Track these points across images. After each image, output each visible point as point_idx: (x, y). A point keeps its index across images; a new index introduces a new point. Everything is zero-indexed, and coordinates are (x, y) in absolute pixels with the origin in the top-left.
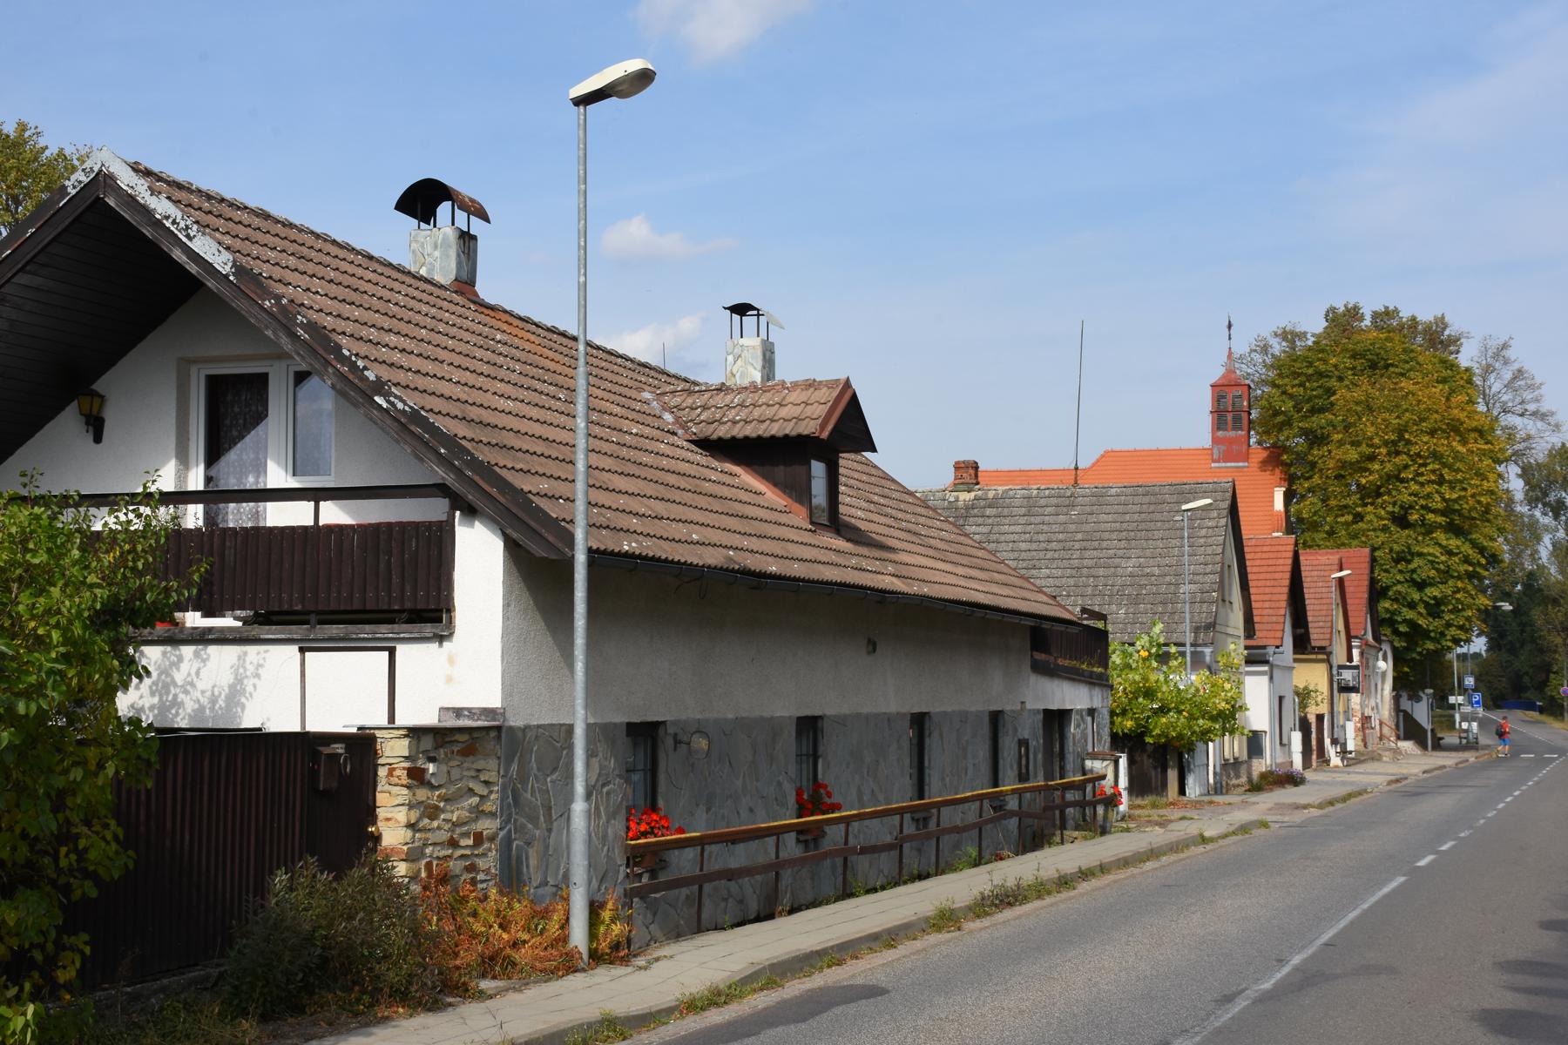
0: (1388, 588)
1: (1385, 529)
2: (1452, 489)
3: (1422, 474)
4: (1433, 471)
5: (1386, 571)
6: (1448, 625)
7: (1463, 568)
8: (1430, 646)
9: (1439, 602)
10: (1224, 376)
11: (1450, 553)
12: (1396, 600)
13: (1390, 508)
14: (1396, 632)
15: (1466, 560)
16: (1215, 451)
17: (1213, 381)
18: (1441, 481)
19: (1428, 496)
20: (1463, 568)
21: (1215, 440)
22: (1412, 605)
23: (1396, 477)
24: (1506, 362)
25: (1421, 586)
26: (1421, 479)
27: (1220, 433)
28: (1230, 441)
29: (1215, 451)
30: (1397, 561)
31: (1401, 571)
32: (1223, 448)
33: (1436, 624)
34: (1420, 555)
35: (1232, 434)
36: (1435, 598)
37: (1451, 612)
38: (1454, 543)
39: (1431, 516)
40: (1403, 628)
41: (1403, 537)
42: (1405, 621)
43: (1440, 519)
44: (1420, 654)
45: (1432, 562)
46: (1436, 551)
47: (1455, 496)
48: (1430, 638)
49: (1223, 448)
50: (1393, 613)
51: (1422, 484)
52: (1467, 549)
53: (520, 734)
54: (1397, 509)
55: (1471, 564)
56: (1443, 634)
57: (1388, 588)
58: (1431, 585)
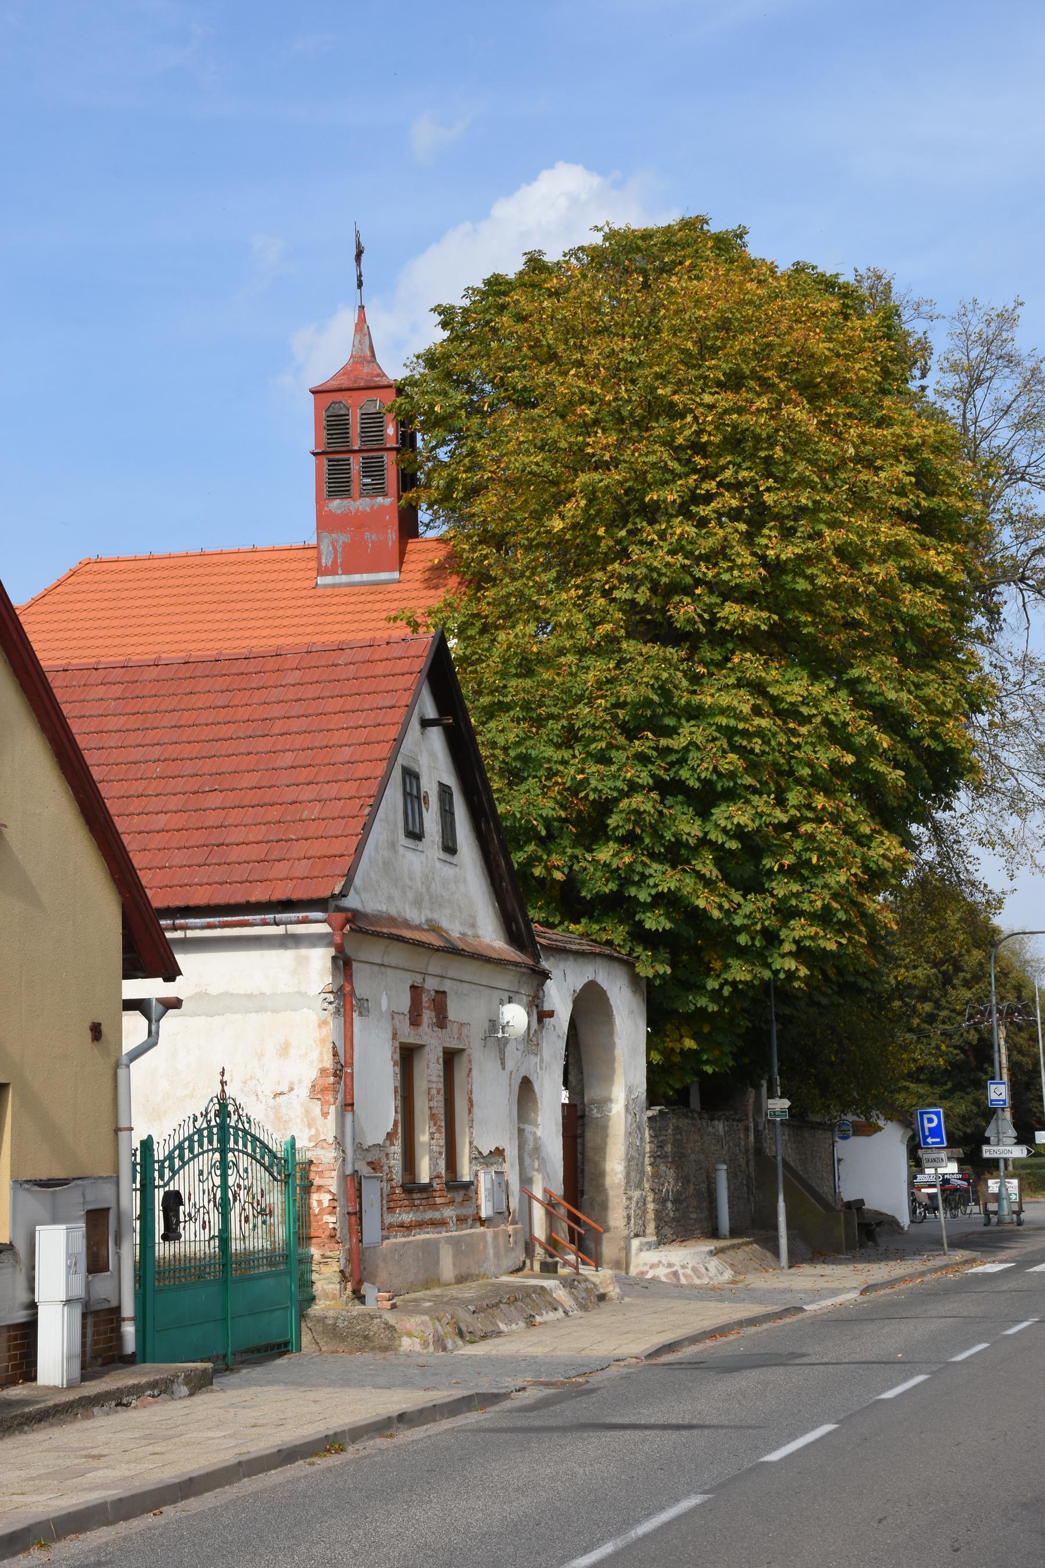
0: (605, 807)
1: (608, 646)
2: (787, 534)
3: (708, 498)
4: (736, 486)
5: (603, 759)
6: (786, 912)
7: (826, 755)
8: (740, 972)
9: (753, 844)
10: (344, 372)
11: (789, 714)
12: (630, 840)
13: (623, 593)
14: (641, 936)
15: (836, 734)
16: (326, 547)
17: (317, 382)
18: (757, 516)
19: (718, 555)
20: (826, 755)
21: (325, 523)
22: (676, 854)
23: (633, 508)
24: (1010, 360)
25: (704, 800)
26: (703, 511)
27: (336, 505)
28: (358, 523)
29: (326, 547)
30: (631, 733)
31: (642, 759)
32: (343, 538)
33: (750, 908)
34: (696, 713)
35: (363, 504)
36: (739, 834)
37: (791, 872)
38: (794, 686)
39: (731, 611)
40: (654, 922)
41: (650, 664)
42: (660, 900)
43: (751, 616)
44: (716, 995)
45: (729, 732)
46: (744, 702)
47: (789, 552)
48: (742, 952)
49: (343, 538)
50: (625, 878)
51: (702, 523)
52: (840, 707)
53: (667, 1231)
54: (642, 597)
55: (848, 746)
56: (772, 938)
57: (605, 807)
58: (730, 795)
